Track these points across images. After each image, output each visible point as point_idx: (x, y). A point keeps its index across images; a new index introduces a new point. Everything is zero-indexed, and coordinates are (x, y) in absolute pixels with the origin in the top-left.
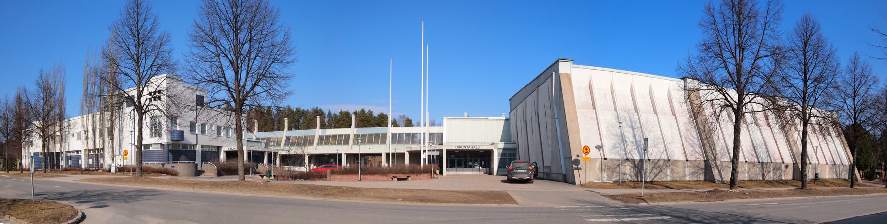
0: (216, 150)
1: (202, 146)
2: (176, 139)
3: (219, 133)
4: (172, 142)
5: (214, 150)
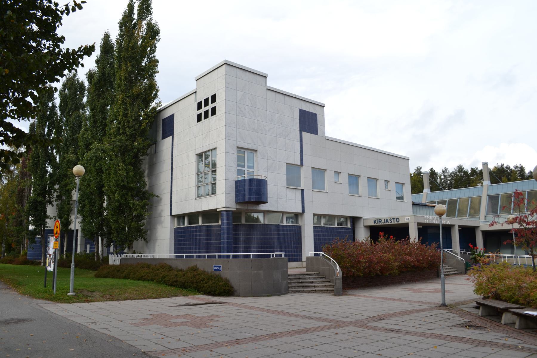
4: (238, 207)
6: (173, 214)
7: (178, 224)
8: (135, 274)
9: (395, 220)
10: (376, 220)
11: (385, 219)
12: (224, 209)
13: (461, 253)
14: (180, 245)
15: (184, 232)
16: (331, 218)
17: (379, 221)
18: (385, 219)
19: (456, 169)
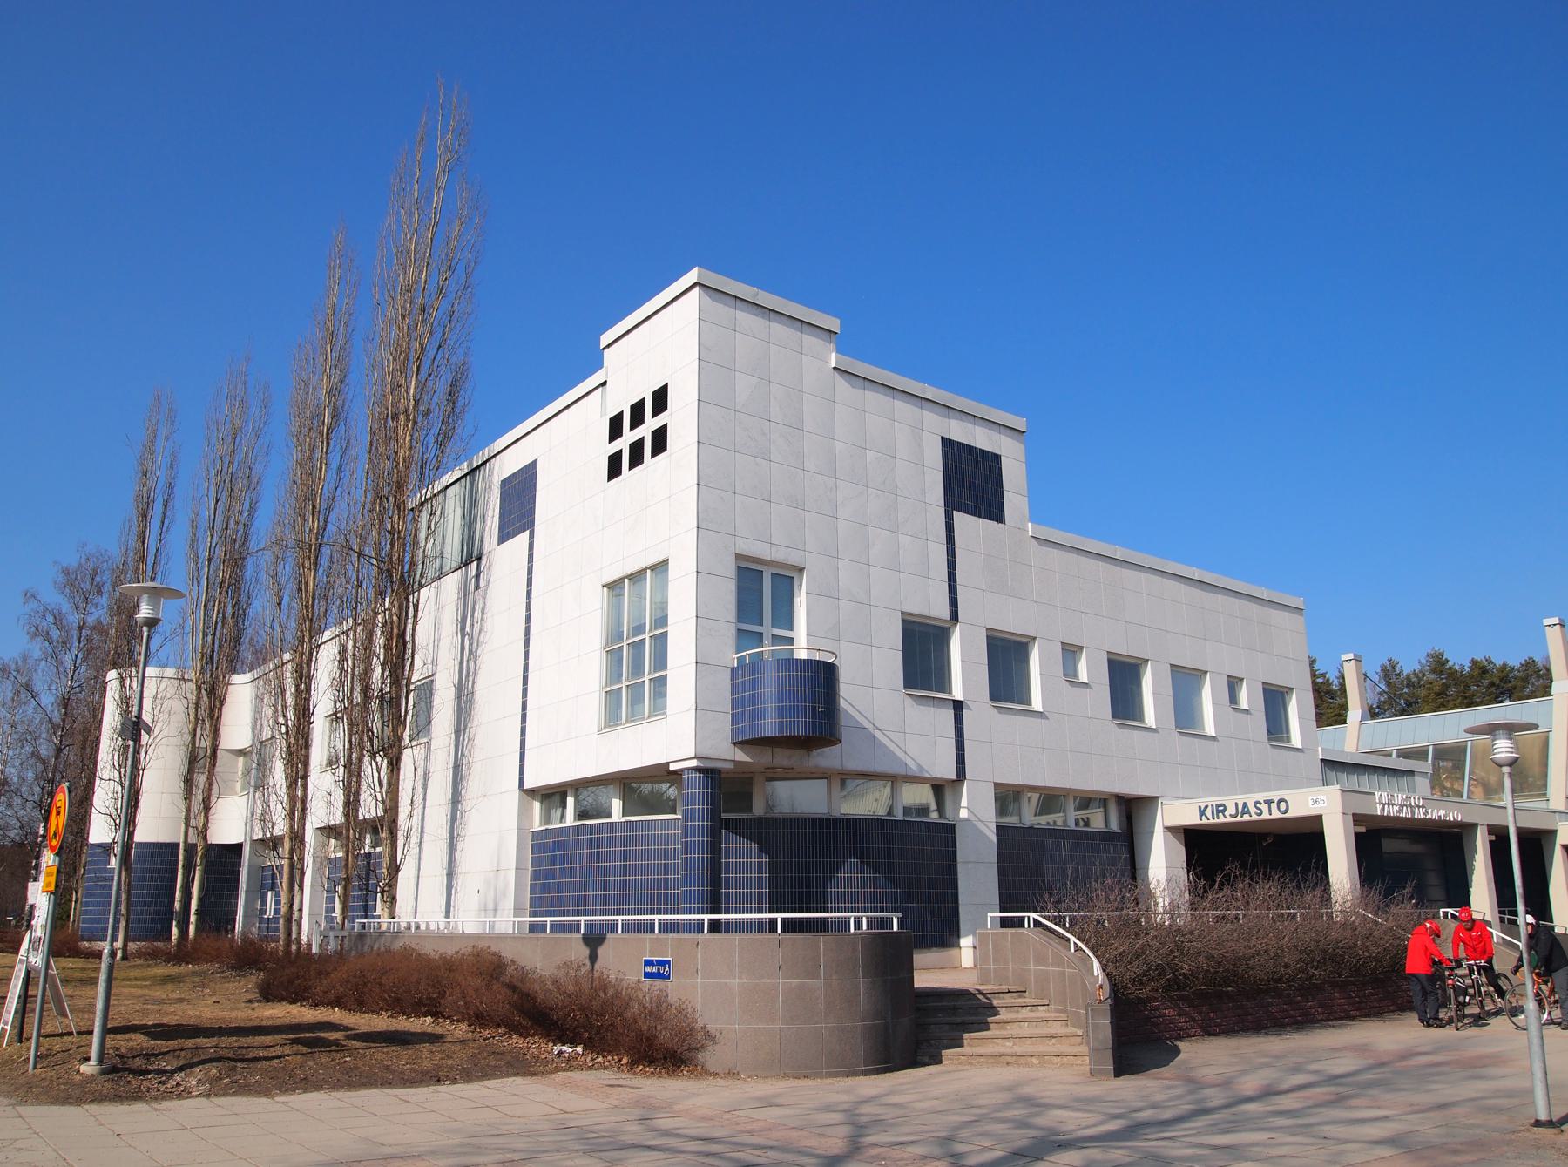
0: (1115, 826)
1: (1007, 797)
2: (770, 726)
3: (1125, 703)
4: (741, 756)
5: (1097, 823)
6: (526, 786)
7: (546, 819)
8: (1148, 934)
9: (1274, 806)
10: (1207, 807)
11: (1236, 804)
12: (694, 763)
13: (1502, 920)
14: (547, 888)
15: (562, 845)
16: (1051, 799)
17: (1218, 812)
18: (1236, 804)
19: (1424, 661)
